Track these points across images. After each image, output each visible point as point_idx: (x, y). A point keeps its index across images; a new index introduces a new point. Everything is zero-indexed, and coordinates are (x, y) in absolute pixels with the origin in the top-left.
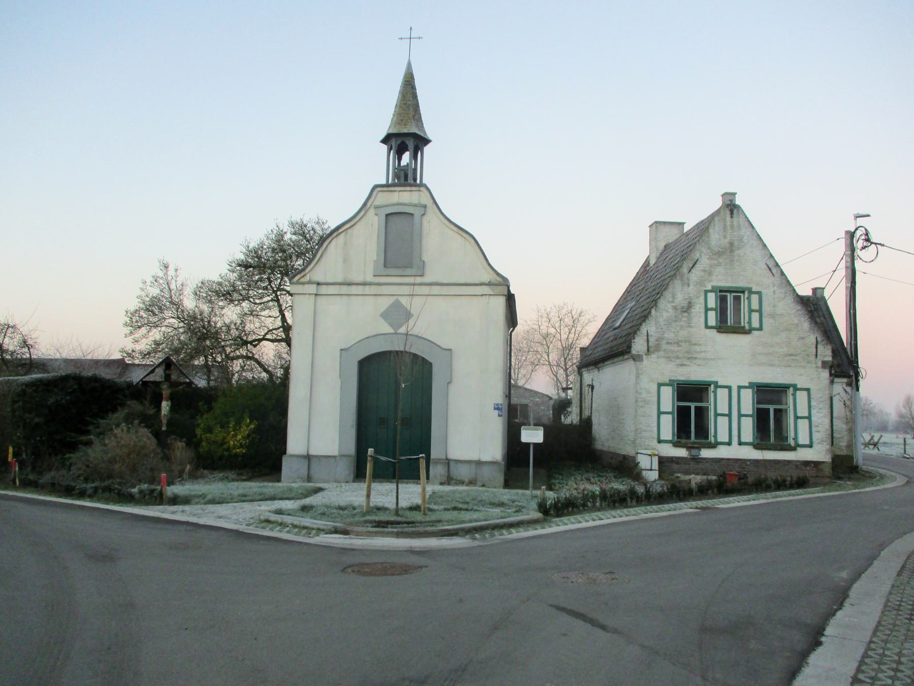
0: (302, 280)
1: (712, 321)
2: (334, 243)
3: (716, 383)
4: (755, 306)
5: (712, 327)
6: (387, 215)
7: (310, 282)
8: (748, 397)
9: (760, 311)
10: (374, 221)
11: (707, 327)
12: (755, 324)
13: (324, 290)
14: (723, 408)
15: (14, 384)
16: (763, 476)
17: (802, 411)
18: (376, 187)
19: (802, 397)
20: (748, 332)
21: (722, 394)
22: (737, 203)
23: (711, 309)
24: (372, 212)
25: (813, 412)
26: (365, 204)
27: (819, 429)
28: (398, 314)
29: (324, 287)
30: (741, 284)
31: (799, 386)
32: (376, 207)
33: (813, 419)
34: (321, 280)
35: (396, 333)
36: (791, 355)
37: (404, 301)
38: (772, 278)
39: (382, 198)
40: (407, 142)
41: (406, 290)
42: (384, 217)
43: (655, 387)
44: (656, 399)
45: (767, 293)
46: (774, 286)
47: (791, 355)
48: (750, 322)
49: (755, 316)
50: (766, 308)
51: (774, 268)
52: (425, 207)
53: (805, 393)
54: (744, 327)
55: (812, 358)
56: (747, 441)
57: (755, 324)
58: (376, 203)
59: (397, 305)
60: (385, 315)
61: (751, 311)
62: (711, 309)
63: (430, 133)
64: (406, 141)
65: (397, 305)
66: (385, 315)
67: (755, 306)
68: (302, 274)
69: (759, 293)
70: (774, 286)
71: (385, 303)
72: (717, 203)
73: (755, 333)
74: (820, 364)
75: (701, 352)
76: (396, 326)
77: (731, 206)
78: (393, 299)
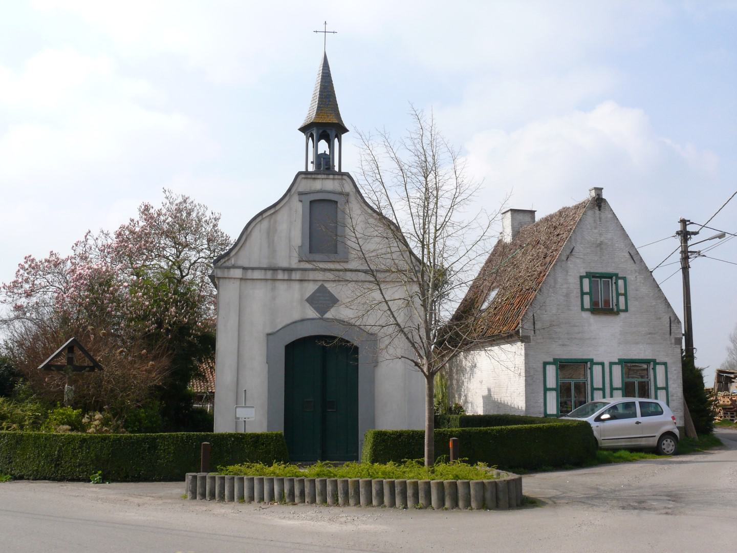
0: (227, 264)
1: (587, 304)
2: (258, 226)
3: (591, 361)
4: (622, 291)
5: (587, 310)
6: (311, 202)
7: (234, 267)
8: (617, 371)
9: (625, 295)
10: (298, 208)
11: (583, 309)
12: (622, 307)
13: (250, 274)
14: (598, 383)
15: (505, 432)
16: (362, 461)
17: (661, 383)
18: (300, 173)
19: (660, 370)
20: (617, 313)
21: (597, 369)
22: (604, 197)
23: (586, 293)
24: (296, 198)
25: (670, 383)
26: (289, 190)
27: (674, 398)
28: (322, 300)
29: (250, 272)
30: (610, 270)
31: (620, 276)
32: (300, 194)
33: (670, 389)
34: (246, 265)
35: (320, 319)
36: (650, 334)
37: (330, 286)
38: (634, 265)
39: (305, 185)
40: (329, 132)
41: (330, 276)
42: (309, 203)
43: (541, 365)
44: (719, 460)
45: (631, 278)
46: (636, 272)
47: (650, 334)
48: (617, 305)
49: (622, 299)
50: (631, 293)
51: (634, 256)
52: (348, 195)
53: (663, 367)
54: (612, 309)
55: (668, 336)
56: (551, 387)
57: (622, 307)
58: (300, 190)
59: (322, 290)
60: (311, 300)
61: (618, 295)
62: (586, 293)
63: (347, 124)
64: (326, 126)
65: (322, 290)
66: (311, 300)
67: (622, 291)
68: (226, 259)
69: (624, 279)
70: (636, 272)
71: (311, 288)
72: (586, 195)
73: (622, 315)
74: (673, 341)
75: (579, 333)
76: (322, 310)
77: (598, 202)
78: (320, 284)
